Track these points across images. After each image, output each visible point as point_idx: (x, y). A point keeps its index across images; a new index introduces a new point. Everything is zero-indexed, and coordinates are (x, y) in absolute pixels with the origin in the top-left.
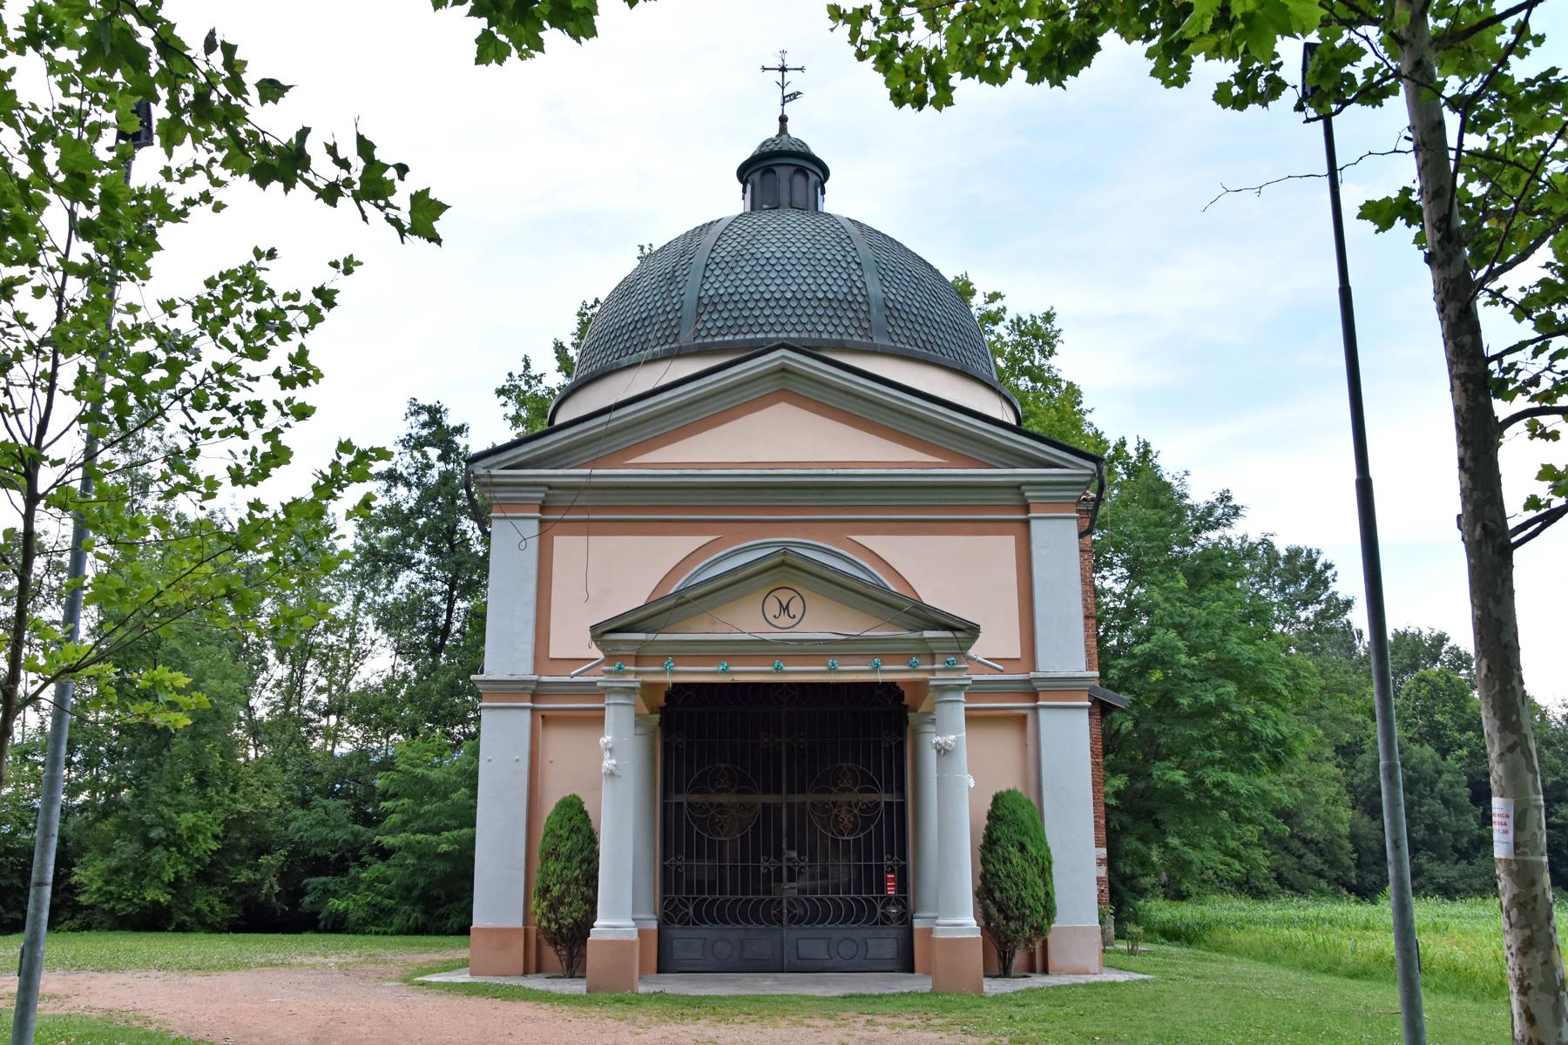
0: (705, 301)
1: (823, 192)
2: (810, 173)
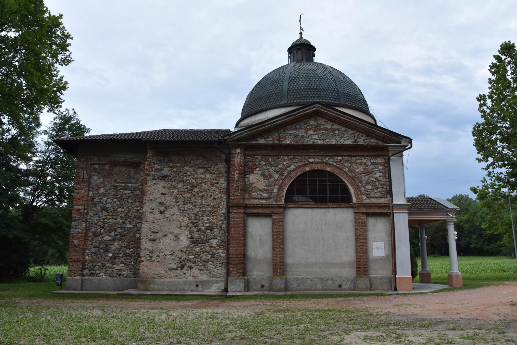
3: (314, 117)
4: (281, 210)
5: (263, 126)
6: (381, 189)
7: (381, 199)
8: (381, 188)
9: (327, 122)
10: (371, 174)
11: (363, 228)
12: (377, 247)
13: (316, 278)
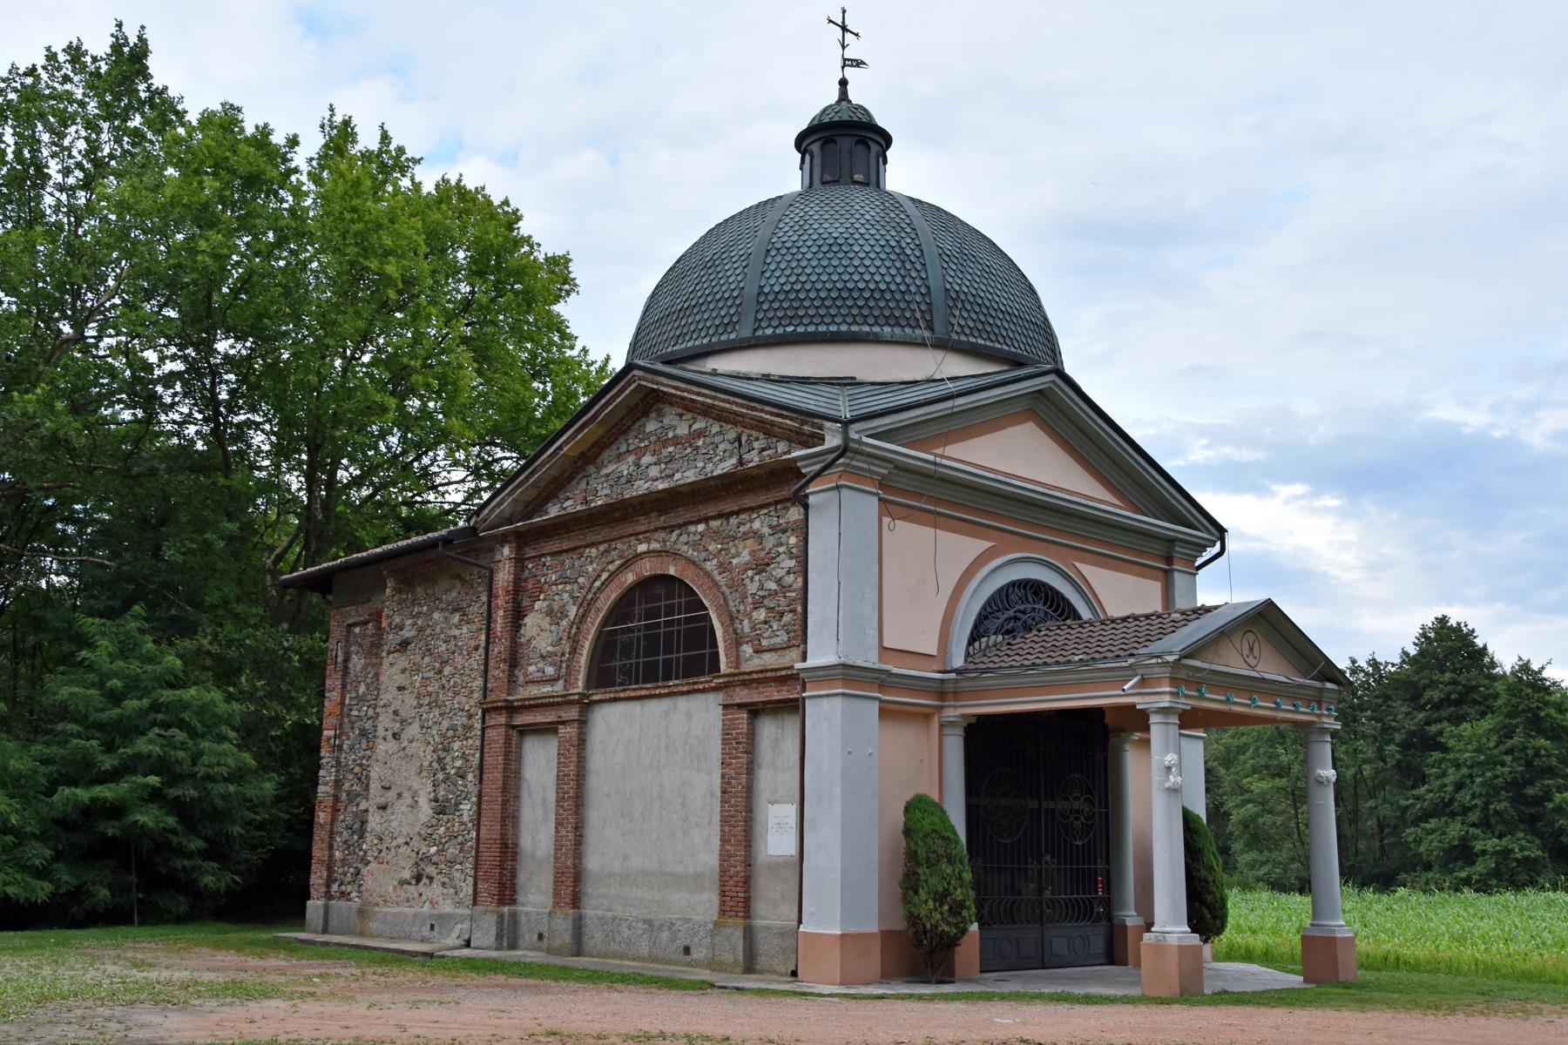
0: (766, 290)
1: (885, 162)
2: (872, 145)
3: (655, 407)
4: (572, 713)
5: (534, 470)
6: (790, 615)
7: (787, 651)
8: (791, 611)
9: (681, 415)
10: (768, 569)
11: (740, 758)
12: (777, 821)
13: (638, 921)
